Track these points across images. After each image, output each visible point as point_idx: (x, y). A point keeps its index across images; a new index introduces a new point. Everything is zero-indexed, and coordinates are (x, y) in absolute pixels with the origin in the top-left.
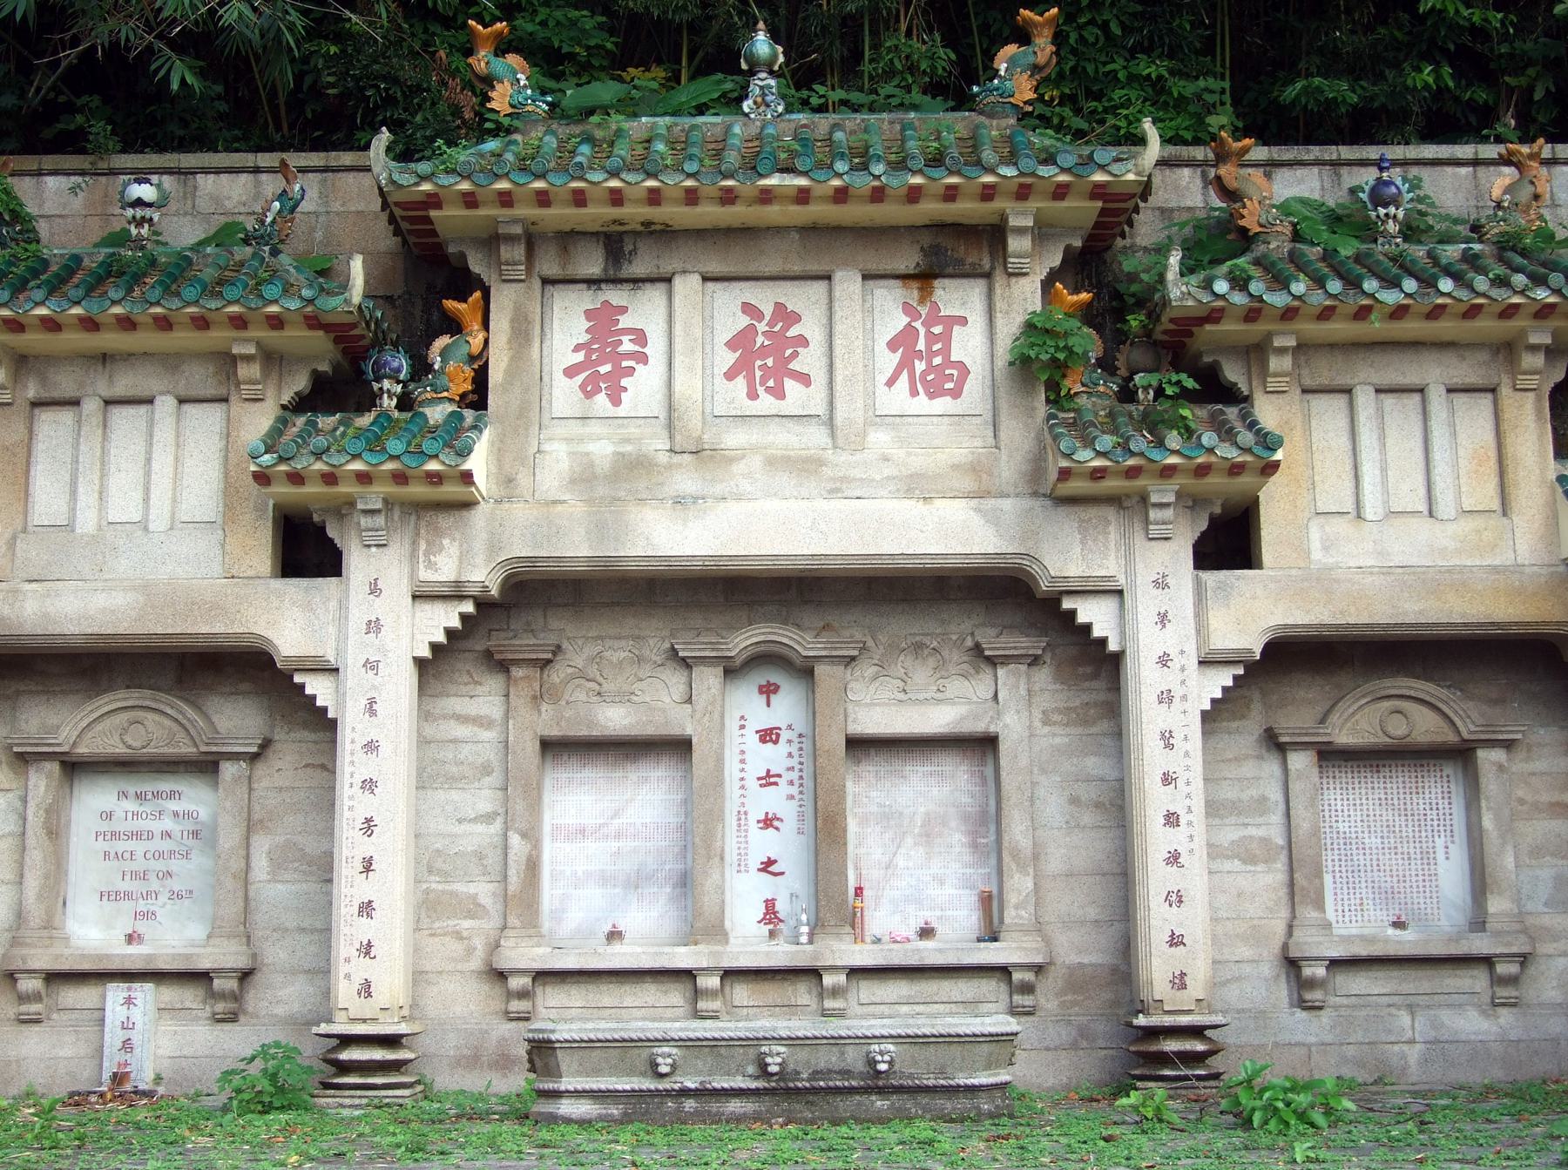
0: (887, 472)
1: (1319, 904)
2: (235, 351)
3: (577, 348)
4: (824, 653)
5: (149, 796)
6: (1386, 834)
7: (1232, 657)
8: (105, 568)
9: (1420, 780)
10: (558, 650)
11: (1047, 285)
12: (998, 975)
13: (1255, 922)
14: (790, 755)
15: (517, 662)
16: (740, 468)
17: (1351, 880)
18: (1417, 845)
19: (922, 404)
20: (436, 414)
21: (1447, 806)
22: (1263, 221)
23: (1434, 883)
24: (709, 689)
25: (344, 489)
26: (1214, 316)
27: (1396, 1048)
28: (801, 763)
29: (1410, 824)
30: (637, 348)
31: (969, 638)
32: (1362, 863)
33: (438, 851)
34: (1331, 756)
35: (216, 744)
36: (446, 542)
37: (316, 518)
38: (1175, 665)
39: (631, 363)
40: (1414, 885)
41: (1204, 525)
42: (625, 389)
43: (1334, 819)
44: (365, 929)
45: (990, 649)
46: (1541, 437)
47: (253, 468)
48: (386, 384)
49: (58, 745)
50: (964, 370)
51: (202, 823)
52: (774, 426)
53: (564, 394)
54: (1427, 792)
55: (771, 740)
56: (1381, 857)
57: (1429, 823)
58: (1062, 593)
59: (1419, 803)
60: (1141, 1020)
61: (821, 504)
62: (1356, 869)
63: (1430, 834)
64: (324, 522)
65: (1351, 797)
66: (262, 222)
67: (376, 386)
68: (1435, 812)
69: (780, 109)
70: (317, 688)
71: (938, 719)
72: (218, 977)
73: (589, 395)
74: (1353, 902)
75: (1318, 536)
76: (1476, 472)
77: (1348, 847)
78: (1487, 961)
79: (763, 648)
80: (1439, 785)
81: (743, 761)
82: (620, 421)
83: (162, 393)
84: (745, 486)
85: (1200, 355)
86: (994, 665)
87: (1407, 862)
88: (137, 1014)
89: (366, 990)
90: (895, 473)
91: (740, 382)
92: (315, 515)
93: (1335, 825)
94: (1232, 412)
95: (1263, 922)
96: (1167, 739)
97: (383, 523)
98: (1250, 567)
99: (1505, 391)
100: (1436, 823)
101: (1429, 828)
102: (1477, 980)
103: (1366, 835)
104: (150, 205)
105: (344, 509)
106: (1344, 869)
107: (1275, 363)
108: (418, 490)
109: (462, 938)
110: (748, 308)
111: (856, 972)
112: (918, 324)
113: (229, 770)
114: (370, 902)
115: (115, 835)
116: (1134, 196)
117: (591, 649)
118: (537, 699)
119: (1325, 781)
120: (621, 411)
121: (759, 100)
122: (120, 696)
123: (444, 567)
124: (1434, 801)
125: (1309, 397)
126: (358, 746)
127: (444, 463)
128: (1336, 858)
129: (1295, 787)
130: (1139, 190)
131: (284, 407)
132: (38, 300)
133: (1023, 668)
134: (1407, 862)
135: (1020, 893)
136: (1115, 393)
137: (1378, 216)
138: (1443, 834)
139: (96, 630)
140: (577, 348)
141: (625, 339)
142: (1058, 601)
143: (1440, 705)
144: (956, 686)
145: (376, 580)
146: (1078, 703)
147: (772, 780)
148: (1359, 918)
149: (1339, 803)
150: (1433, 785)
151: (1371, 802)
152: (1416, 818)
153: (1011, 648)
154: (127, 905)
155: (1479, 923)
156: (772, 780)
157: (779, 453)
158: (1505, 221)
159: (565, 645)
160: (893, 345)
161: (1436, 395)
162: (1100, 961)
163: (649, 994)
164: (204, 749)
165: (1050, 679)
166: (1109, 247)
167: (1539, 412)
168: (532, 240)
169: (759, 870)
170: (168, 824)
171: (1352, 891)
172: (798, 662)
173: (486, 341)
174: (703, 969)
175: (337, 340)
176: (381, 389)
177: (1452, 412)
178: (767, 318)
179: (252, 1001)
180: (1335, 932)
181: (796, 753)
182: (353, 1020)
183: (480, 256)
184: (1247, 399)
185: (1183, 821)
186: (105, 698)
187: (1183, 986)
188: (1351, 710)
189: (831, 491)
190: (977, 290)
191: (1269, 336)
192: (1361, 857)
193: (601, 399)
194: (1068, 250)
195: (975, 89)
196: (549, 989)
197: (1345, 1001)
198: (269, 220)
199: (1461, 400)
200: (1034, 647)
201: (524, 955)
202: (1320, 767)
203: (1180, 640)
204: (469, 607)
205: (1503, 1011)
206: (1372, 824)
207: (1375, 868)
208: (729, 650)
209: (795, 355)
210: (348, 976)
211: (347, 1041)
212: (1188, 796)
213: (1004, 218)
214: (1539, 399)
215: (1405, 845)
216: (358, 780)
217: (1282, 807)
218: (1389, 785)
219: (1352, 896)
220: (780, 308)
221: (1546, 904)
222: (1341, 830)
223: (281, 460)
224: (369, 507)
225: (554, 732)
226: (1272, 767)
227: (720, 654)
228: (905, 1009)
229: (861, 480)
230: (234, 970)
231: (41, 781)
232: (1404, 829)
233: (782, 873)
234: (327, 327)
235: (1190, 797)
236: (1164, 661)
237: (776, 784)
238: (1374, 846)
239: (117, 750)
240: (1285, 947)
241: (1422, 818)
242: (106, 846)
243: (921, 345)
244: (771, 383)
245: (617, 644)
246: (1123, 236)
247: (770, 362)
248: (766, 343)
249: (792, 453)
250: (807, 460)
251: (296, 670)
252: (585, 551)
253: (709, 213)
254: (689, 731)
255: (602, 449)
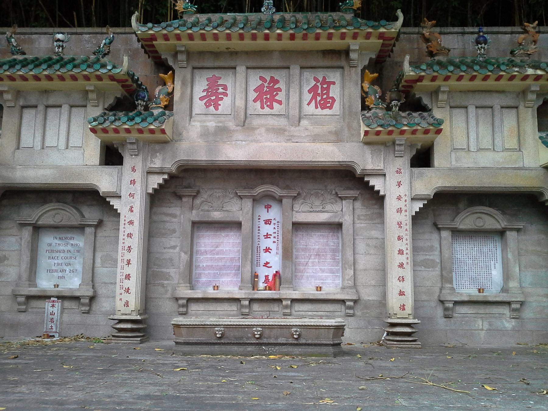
0: (306, 134)
1: (451, 282)
2: (87, 88)
3: (204, 91)
4: (285, 195)
5: (64, 239)
6: (474, 259)
7: (423, 197)
8: (44, 161)
9: (486, 241)
10: (198, 192)
11: (363, 71)
12: (341, 302)
13: (429, 288)
14: (274, 228)
15: (185, 196)
16: (257, 132)
17: (462, 274)
18: (485, 263)
19: (319, 111)
20: (156, 112)
21: (495, 250)
22: (438, 49)
23: (490, 276)
24: (248, 206)
25: (123, 135)
26: (420, 79)
27: (477, 331)
28: (278, 231)
29: (482, 256)
30: (224, 91)
31: (334, 191)
32: (466, 269)
33: (157, 258)
34: (457, 233)
35: (83, 221)
36: (158, 154)
37: (115, 146)
38: (403, 200)
39: (222, 96)
40: (483, 277)
41: (414, 153)
42: (220, 105)
43: (456, 254)
44: (403, 259)
45: (340, 194)
46: (534, 123)
47: (90, 127)
48: (139, 102)
49: (31, 221)
50: (334, 100)
51: (81, 248)
52: (269, 118)
53: (199, 106)
54: (488, 245)
55: (268, 223)
56: (472, 267)
57: (489, 256)
58: (365, 175)
59: (485, 249)
60: (390, 321)
61: (284, 144)
62: (463, 271)
63: (489, 260)
64: (118, 147)
65: (462, 247)
66: (99, 47)
67: (136, 102)
68: (491, 252)
69: (274, 10)
70: (114, 202)
71: (322, 217)
72: (83, 299)
73: (207, 107)
74: (462, 282)
75: (454, 156)
76: (510, 135)
77: (461, 263)
78: (509, 303)
79: (266, 193)
80: (493, 243)
81: (259, 230)
82: (218, 116)
83: (64, 104)
84: (259, 137)
85: (415, 94)
86: (342, 200)
87: (481, 269)
88: (55, 310)
89: (127, 304)
90: (310, 134)
91: (258, 104)
92: (115, 145)
93: (456, 256)
94: (425, 114)
95: (432, 288)
96: (400, 224)
97: (136, 147)
98: (430, 167)
99: (521, 108)
100: (491, 256)
101: (489, 258)
102: (505, 310)
103: (467, 259)
104: (63, 41)
105: (123, 143)
106: (459, 271)
107: (441, 97)
108: (147, 135)
109: (164, 287)
110: (261, 78)
111: (294, 301)
112: (318, 84)
113: (88, 230)
114: (129, 274)
115: (52, 251)
116: (393, 38)
117: (209, 193)
118: (192, 208)
119: (453, 241)
120: (219, 112)
121: (267, 7)
122: (53, 205)
123: (157, 163)
124: (491, 249)
125: (452, 109)
126: (126, 222)
127: (154, 126)
128: (457, 267)
129: (444, 242)
130: (395, 36)
131: (106, 109)
132: (18, 69)
133: (352, 201)
134: (481, 269)
135: (349, 275)
136: (385, 108)
137: (478, 48)
138: (493, 260)
139: (40, 182)
140: (204, 91)
141: (220, 88)
142: (364, 178)
143: (494, 216)
144: (329, 207)
145: (134, 166)
146: (369, 213)
147: (268, 236)
148: (464, 287)
149: (458, 248)
150: (490, 243)
151: (469, 248)
152: (484, 254)
153: (347, 194)
154: (55, 274)
155: (504, 290)
156: (268, 236)
157: (271, 127)
158: (523, 49)
159: (201, 190)
160: (310, 91)
161: (497, 108)
162: (375, 299)
163: (226, 307)
164: (80, 223)
165: (360, 205)
166: (385, 61)
167: (533, 117)
168: (189, 54)
169: (263, 266)
170: (69, 247)
171: (462, 278)
172: (277, 197)
173: (174, 88)
174: (243, 298)
175: (123, 86)
176: (138, 103)
177: (502, 115)
178: (268, 82)
179: (95, 307)
180: (456, 292)
181: (276, 228)
182: (123, 314)
183: (172, 59)
184: (430, 110)
185: (405, 253)
186: (47, 205)
187: (404, 309)
188: (463, 217)
189: (287, 140)
190: (339, 73)
191: (439, 87)
192: (465, 267)
193: (212, 108)
194: (371, 59)
195: (340, 4)
196: (192, 304)
197: (460, 315)
198: (102, 46)
199: (504, 111)
200: (355, 194)
201: (186, 292)
202: (452, 236)
203: (404, 190)
204: (166, 177)
205: (513, 320)
206: (469, 256)
207: (470, 270)
208: (254, 193)
209: (277, 94)
210: (121, 299)
211: (121, 321)
212: (407, 244)
213: (349, 46)
214: (533, 111)
215: (481, 263)
216: (126, 234)
217: (439, 249)
218: (475, 243)
219: (462, 280)
220: (272, 78)
221: (529, 284)
222: (459, 257)
223: (100, 124)
224: (131, 141)
225: (197, 219)
226: (435, 236)
227: (251, 194)
228: (310, 313)
229: (298, 136)
230: (88, 296)
231: (27, 233)
232: (480, 258)
233: (271, 267)
234: (118, 81)
235: (406, 245)
236: (399, 198)
237: (270, 238)
238: (470, 263)
239: (51, 223)
240: (439, 296)
241: (486, 254)
242: (49, 255)
243: (319, 91)
244: (269, 104)
245: (218, 191)
246: (389, 56)
247: (268, 96)
248: (267, 90)
249: (275, 127)
250: (280, 129)
251: (108, 196)
252: (204, 158)
253: (248, 44)
254: (241, 220)
255: (212, 124)
